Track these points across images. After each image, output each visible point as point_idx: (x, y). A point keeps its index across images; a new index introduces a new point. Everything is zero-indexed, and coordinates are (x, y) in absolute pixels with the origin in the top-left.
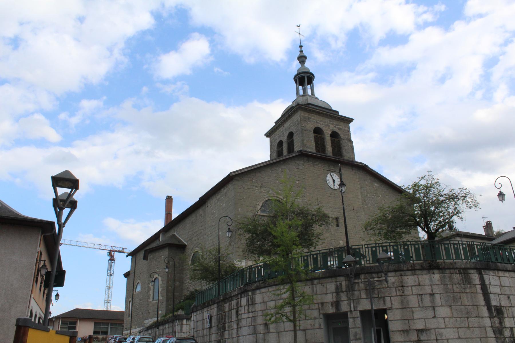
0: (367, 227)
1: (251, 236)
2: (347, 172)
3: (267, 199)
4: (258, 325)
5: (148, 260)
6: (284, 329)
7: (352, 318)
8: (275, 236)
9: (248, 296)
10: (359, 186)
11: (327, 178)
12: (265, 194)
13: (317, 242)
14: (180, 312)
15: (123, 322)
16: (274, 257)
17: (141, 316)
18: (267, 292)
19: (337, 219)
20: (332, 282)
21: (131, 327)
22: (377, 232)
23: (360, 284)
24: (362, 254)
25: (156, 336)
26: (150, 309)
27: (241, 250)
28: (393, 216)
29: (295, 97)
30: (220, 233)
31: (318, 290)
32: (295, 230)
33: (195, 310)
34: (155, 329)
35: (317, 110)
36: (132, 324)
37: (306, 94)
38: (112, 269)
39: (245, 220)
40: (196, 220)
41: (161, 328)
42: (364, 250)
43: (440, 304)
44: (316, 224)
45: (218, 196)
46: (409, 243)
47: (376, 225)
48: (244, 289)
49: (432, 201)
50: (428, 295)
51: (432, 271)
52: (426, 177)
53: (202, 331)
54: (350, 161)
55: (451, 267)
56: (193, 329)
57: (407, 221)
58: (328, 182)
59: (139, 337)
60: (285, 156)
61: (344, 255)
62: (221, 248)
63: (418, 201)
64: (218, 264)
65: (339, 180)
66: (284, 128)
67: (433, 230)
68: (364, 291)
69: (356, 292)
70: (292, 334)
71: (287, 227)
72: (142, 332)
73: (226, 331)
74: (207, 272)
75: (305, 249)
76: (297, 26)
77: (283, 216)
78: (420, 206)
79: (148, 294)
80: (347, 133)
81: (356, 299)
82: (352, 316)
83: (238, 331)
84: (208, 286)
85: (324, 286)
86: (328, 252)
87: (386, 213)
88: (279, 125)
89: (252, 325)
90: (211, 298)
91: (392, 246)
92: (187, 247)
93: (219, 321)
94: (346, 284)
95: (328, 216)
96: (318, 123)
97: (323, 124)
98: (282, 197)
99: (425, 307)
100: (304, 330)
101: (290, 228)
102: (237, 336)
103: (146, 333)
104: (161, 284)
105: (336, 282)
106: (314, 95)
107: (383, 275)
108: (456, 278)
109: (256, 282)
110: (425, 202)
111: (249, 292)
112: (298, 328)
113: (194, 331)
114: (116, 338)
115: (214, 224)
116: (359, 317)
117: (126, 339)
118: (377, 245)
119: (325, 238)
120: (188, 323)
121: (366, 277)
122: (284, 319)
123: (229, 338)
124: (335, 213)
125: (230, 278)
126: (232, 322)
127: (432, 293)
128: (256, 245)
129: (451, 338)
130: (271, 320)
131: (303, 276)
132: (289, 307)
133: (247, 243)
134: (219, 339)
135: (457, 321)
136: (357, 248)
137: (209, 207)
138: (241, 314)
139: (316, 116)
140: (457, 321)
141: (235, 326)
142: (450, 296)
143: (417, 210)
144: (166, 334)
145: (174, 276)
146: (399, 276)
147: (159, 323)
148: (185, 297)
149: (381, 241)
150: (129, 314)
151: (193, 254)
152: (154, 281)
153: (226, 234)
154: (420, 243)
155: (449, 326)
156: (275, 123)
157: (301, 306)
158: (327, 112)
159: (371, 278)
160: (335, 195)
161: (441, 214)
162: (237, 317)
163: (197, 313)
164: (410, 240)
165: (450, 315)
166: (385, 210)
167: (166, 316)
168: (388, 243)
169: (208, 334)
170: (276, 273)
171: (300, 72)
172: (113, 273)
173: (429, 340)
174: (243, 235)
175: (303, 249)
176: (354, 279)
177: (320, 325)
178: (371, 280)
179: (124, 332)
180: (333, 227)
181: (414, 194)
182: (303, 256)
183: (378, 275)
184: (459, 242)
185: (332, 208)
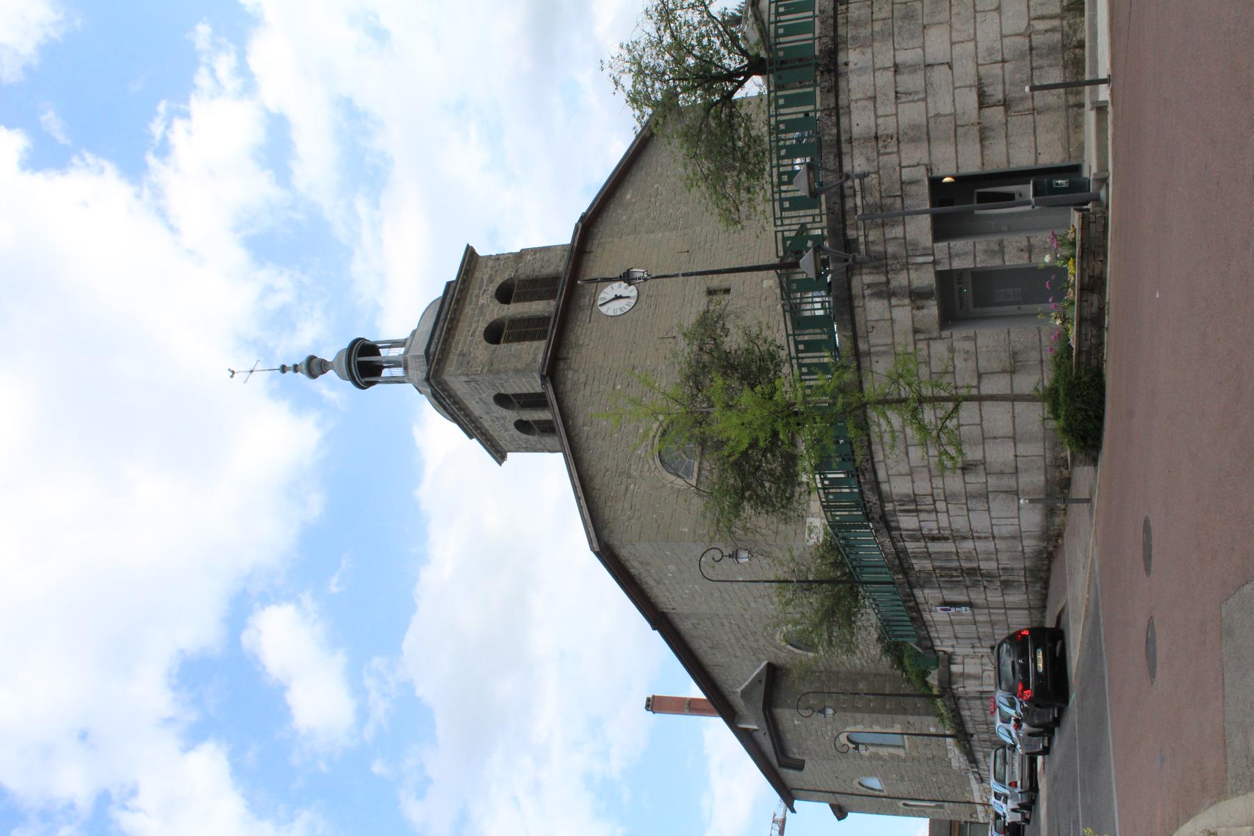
0: (733, 219)
1: (749, 501)
2: (597, 265)
4: (965, 488)
5: (804, 758)
6: (976, 424)
9: (895, 511)
10: (631, 237)
11: (611, 313)
12: (646, 467)
13: (765, 341)
15: (955, 821)
16: (802, 448)
17: (942, 776)
18: (886, 465)
19: (711, 292)
20: (864, 306)
21: (969, 802)
22: (744, 195)
23: (871, 238)
24: (796, 234)
25: (991, 741)
26: (925, 754)
27: (782, 527)
29: (409, 388)
30: (741, 579)
31: (883, 341)
33: (929, 644)
34: (972, 743)
35: (443, 333)
36: (960, 800)
37: (401, 359)
41: (970, 727)
42: (787, 228)
43: (920, 51)
44: (723, 342)
46: (773, 121)
47: (727, 198)
48: (878, 522)
50: (898, 78)
54: (570, 259)
55: (831, 21)
56: (973, 647)
57: (720, 124)
58: (619, 313)
59: (993, 781)
60: (554, 415)
61: (799, 276)
62: (776, 577)
63: (671, 95)
64: (817, 585)
65: (616, 285)
66: (485, 416)
67: (742, 61)
68: (887, 230)
69: (890, 250)
70: (987, 405)
71: (729, 413)
72: (979, 775)
74: (834, 612)
75: (784, 371)
76: (232, 377)
77: (701, 424)
78: (685, 90)
80: (503, 262)
82: (947, 261)
83: (979, 538)
84: (869, 610)
85: (873, 327)
88: (477, 428)
90: (901, 603)
92: (774, 661)
93: (954, 584)
94: (870, 273)
96: (474, 332)
97: (478, 321)
98: (655, 426)
99: (926, 86)
101: (731, 406)
103: (982, 766)
105: (864, 297)
106: (406, 340)
107: (849, 183)
108: (857, 12)
110: (674, 80)
112: (974, 392)
113: (979, 645)
115: (717, 594)
116: (949, 244)
117: (997, 816)
119: (755, 322)
120: (959, 660)
121: (852, 224)
122: (951, 424)
123: (997, 560)
126: (957, 552)
127: (892, 69)
128: (770, 490)
129: (999, 29)
130: (954, 455)
133: (767, 512)
134: (999, 584)
135: (959, 14)
139: (456, 338)
140: (959, 14)
141: (968, 545)
142: (900, 27)
143: (693, 98)
144: (986, 715)
145: (842, 693)
146: (852, 147)
147: (959, 731)
148: (895, 666)
149: (766, 188)
150: (936, 807)
151: (789, 647)
153: (742, 564)
155: (972, 31)
156: (471, 437)
159: (856, 213)
161: (705, 41)
162: (946, 539)
163: (936, 638)
164: (764, 117)
165: (946, 28)
166: (691, 175)
170: (841, 441)
173: (1004, 80)
177: (967, 338)
178: (860, 212)
179: (981, 821)
180: (732, 303)
181: (656, 104)
182: (800, 376)
184: (772, 23)
185: (683, 305)
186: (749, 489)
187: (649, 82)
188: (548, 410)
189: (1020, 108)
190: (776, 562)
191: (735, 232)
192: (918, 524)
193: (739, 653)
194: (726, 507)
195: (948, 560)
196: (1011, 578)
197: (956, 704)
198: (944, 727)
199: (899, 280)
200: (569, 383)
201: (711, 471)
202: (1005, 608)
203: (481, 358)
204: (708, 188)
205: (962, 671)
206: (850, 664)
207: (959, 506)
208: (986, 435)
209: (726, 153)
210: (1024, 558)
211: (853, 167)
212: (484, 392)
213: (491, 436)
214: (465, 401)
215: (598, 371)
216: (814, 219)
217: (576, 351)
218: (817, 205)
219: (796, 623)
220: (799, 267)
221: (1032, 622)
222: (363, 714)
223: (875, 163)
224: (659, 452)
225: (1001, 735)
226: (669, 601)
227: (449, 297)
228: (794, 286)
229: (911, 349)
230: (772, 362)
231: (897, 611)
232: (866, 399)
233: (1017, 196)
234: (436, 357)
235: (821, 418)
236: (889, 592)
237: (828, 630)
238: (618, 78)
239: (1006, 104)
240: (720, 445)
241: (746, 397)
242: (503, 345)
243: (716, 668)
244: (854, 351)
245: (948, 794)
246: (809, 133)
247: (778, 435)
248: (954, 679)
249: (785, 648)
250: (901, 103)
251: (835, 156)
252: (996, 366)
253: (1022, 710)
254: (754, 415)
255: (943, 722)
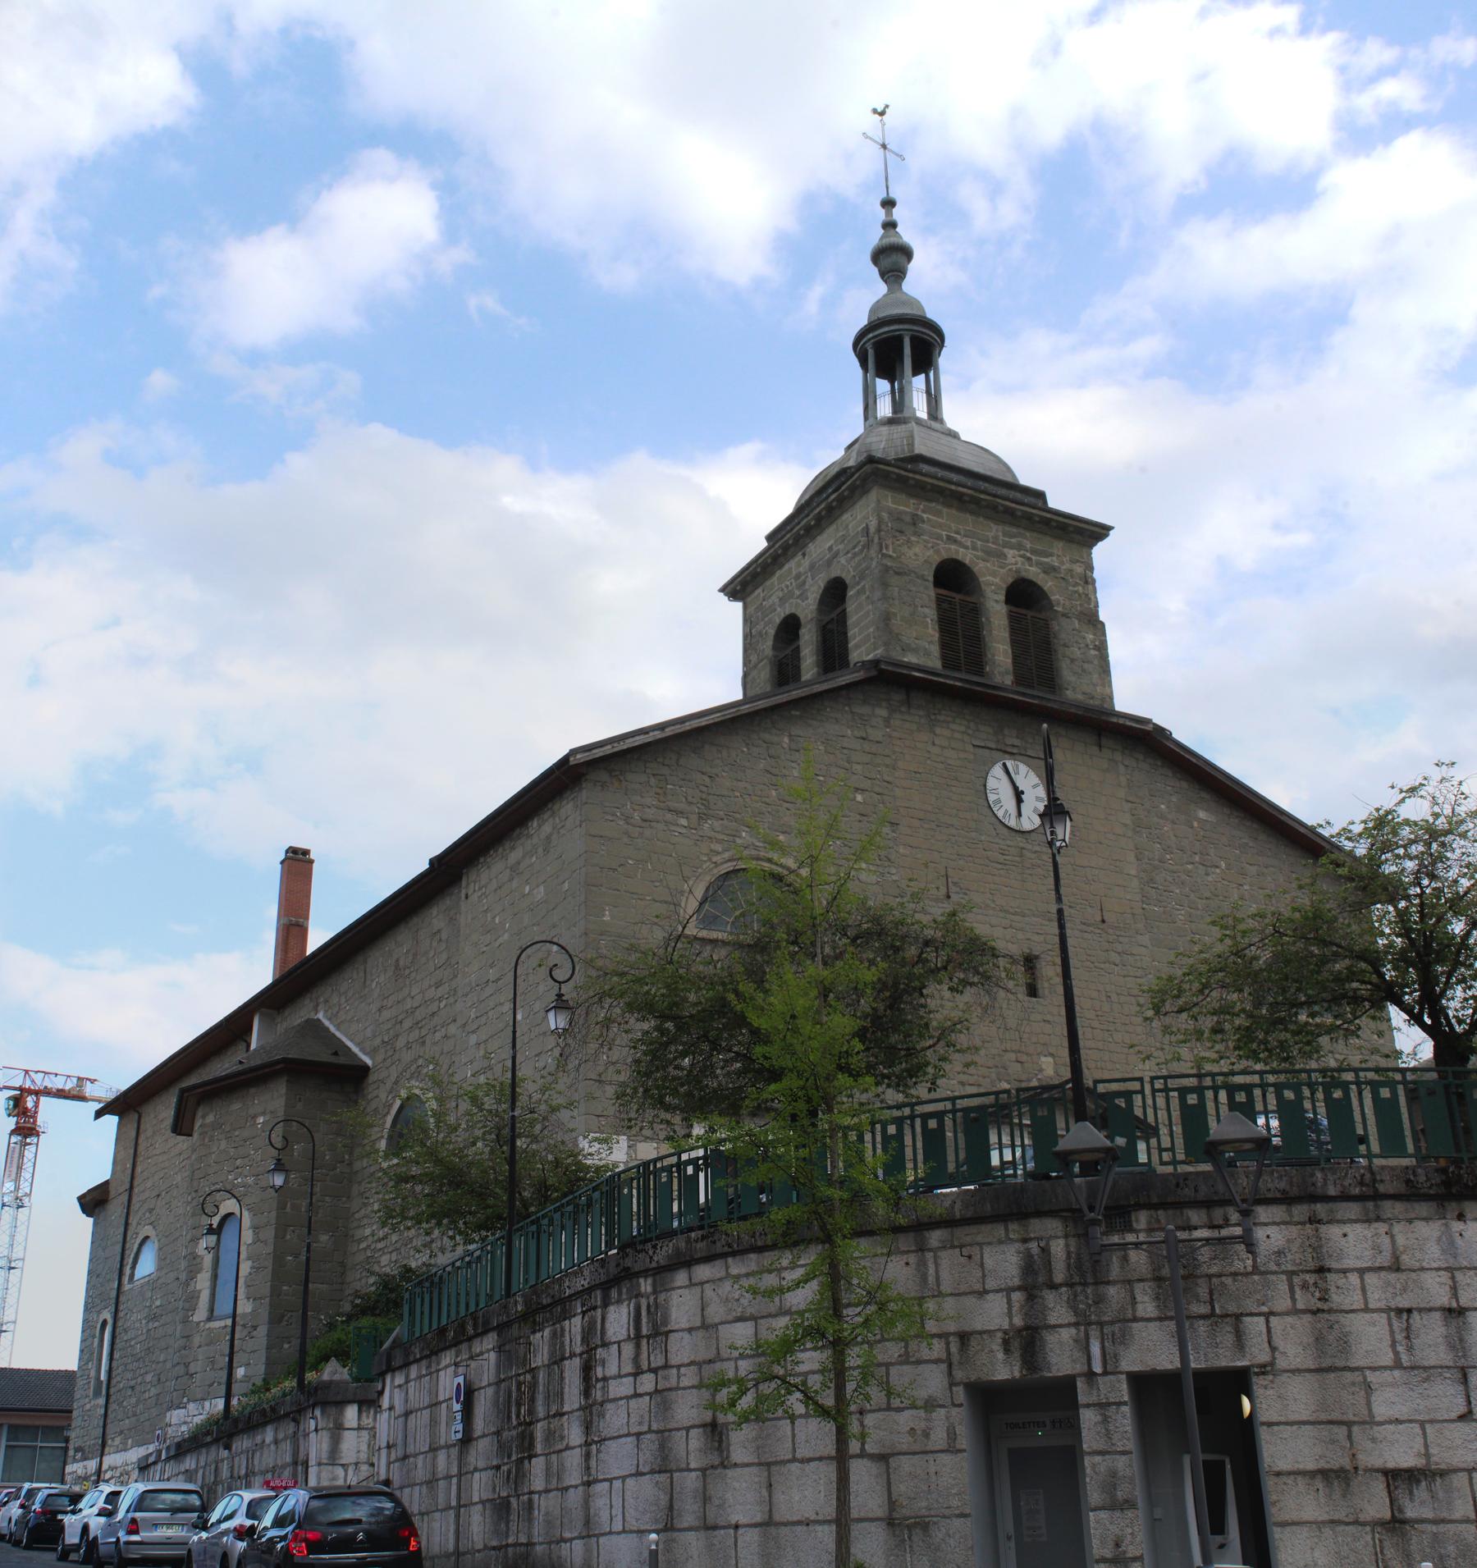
0: (1164, 1001)
1: (657, 1028)
2: (1071, 756)
3: (729, 867)
4: (678, 1429)
5: (196, 1135)
7: (1094, 1405)
8: (759, 1029)
9: (638, 1295)
10: (1127, 819)
11: (991, 783)
12: (718, 848)
13: (943, 1059)
14: (333, 1372)
15: (70, 1418)
16: (750, 1124)
17: (153, 1391)
18: (720, 1279)
19: (1030, 962)
21: (104, 1445)
22: (1208, 1023)
23: (1133, 1255)
24: (1137, 1118)
25: (216, 1483)
27: (610, 1090)
28: (1275, 955)
29: (853, 426)
30: (519, 1017)
31: (945, 1275)
32: (848, 1005)
33: (396, 1363)
34: (213, 1449)
35: (953, 487)
36: (109, 1426)
37: (906, 414)
38: (26, 1175)
39: (633, 957)
40: (415, 955)
41: (242, 1443)
42: (1149, 1101)
44: (940, 982)
45: (515, 853)
46: (1349, 1077)
47: (1201, 991)
48: (618, 1265)
49: (1458, 893)
50: (1437, 1315)
51: (1454, 1204)
52: (1430, 789)
53: (430, 1455)
54: (1087, 709)
56: (389, 1447)
57: (1338, 979)
58: (992, 798)
59: (142, 1487)
60: (809, 684)
61: (1060, 1123)
62: (523, 1080)
63: (1392, 890)
64: (507, 1155)
65: (1041, 792)
66: (806, 563)
67: (1460, 1022)
69: (1112, 1291)
70: (829, 1471)
71: (814, 993)
72: (155, 1463)
73: (536, 1456)
74: (458, 1186)
75: (890, 1091)
76: (875, 111)
77: (793, 943)
78: (1402, 915)
79: (191, 1288)
80: (1080, 589)
81: (1112, 1323)
82: (1094, 1399)
83: (588, 1456)
84: (460, 1250)
85: (970, 1257)
86: (991, 1106)
87: (1247, 941)
89: (650, 1431)
90: (472, 1309)
91: (1271, 1089)
92: (372, 1078)
93: (503, 1409)
94: (1069, 1253)
95: (994, 949)
96: (955, 541)
97: (974, 548)
98: (790, 863)
99: (1425, 1368)
100: (883, 1458)
101: (826, 996)
102: (585, 1478)
103: (171, 1467)
104: (250, 1241)
105: (1025, 1241)
106: (942, 421)
107: (1235, 1217)
109: (672, 1234)
110: (1421, 896)
111: (642, 1280)
112: (854, 1447)
113: (393, 1457)
114: (31, 1494)
115: (492, 974)
116: (1125, 1403)
117: (76, 1498)
118: (1208, 1081)
119: (978, 1043)
120: (367, 1421)
121: (1158, 1221)
122: (795, 1402)
123: (547, 1491)
124: (1020, 935)
125: (557, 1216)
126: (563, 1414)
127: (1454, 1305)
128: (677, 1067)
130: (739, 1408)
131: (881, 1212)
132: (815, 1349)
133: (637, 1062)
134: (504, 1494)
136: (1119, 1094)
137: (474, 898)
138: (605, 1379)
139: (945, 510)
141: (575, 1434)
143: (1387, 931)
144: (264, 1473)
145: (311, 1204)
146: (1303, 1223)
147: (236, 1421)
148: (358, 1301)
149: (1222, 1062)
151: (398, 1103)
152: (216, 1231)
153: (546, 1018)
154: (1398, 1077)
156: (769, 538)
157: (871, 1344)
158: (995, 496)
159: (1179, 1228)
160: (1021, 856)
162: (586, 1393)
163: (407, 1377)
164: (1355, 1060)
166: (1242, 927)
167: (268, 1390)
168: (1255, 1072)
169: (455, 1471)
170: (764, 1198)
171: (881, 315)
172: (27, 1190)
173: (1443, 1521)
174: (619, 1024)
175: (880, 1089)
176: (1103, 1228)
177: (952, 1435)
178: (1181, 1235)
179: (69, 1469)
180: (1011, 1002)
181: (1373, 861)
182: (880, 1121)
183: (1209, 1216)
185: (1006, 912)
186: (678, 1028)
187: (1415, 849)
188: (819, 674)
189: (1389, 1552)
190: (550, 1079)
191: (1139, 1005)
192: (614, 1339)
193: (386, 1014)
194: (646, 988)
195: (548, 1397)
196: (514, 1517)
197: (286, 1415)
198: (245, 1395)
199: (1057, 1309)
200: (865, 710)
201: (710, 962)
202: (459, 1506)
203: (910, 553)
204: (1220, 956)
205: (347, 1425)
206: (366, 1216)
207: (647, 1418)
208: (773, 1468)
209: (1284, 991)
210: (550, 1543)
211: (1266, 1224)
212: (849, 561)
213: (773, 574)
214: (834, 526)
215: (888, 761)
216: (1166, 1150)
217: (923, 721)
218: (1192, 1155)
219: (439, 1116)
220: (1077, 1122)
221: (432, 1558)
222: (255, 358)
223: (1275, 1268)
224: (744, 869)
225: (228, 1499)
226: (480, 889)
227: (1019, 496)
228: (1042, 1112)
229: (931, 1326)
230: (907, 1070)
231: (458, 1302)
232: (839, 1241)
233: (1219, 1539)
234: (911, 475)
235: (804, 1159)
236: (492, 1288)
237: (426, 1174)
238: (1422, 793)
239: (1396, 1524)
240: (758, 977)
241: (842, 1023)
242: (930, 592)
243: (362, 974)
244: (926, 1220)
245: (120, 1404)
246: (1327, 1143)
247: (776, 1081)
248: (333, 1410)
249: (394, 1098)
250: (1389, 1319)
251: (1284, 1192)
252: (901, 1488)
253: (271, 1539)
254: (810, 1038)
255: (253, 1392)
